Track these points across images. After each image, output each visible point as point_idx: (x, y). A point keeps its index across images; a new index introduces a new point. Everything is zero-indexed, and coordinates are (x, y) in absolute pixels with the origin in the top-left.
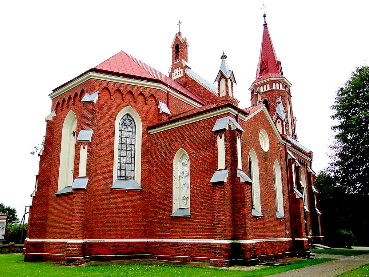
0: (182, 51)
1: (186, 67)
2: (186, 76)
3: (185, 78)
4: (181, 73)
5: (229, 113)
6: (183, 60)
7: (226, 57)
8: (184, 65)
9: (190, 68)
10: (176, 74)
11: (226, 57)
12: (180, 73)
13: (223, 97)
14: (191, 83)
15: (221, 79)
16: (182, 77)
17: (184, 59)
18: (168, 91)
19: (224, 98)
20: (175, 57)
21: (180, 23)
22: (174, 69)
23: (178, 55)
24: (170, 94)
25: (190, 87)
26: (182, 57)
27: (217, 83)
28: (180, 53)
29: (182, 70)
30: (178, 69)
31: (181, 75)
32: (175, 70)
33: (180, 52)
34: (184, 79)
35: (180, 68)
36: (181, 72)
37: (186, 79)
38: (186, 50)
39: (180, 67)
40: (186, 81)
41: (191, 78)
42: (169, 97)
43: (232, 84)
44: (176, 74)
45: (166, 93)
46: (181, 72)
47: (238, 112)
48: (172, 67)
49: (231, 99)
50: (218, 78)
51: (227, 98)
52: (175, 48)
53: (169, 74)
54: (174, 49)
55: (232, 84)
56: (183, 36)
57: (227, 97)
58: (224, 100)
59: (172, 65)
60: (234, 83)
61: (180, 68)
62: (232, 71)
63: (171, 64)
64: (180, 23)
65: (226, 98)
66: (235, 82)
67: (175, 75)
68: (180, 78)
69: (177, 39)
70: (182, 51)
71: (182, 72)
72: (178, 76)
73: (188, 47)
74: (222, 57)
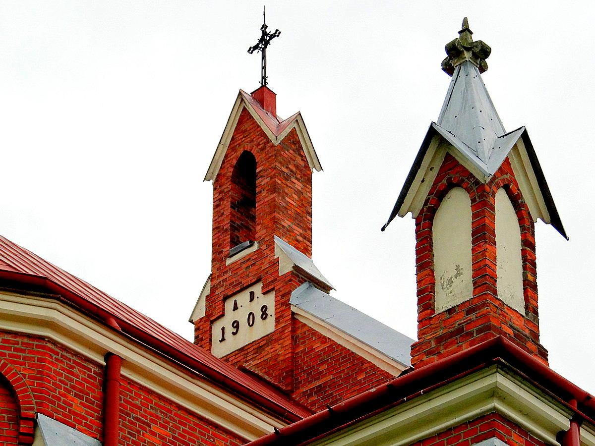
0: (274, 189)
1: (300, 276)
2: (294, 331)
3: (288, 342)
4: (264, 316)
5: (496, 414)
6: (277, 240)
7: (482, 53)
8: (285, 268)
9: (326, 288)
10: (236, 325)
11: (482, 53)
12: (258, 314)
13: (450, 311)
14: (326, 366)
15: (438, 196)
16: (268, 340)
17: (287, 234)
18: (109, 356)
19: (460, 320)
20: (233, 228)
21: (266, 38)
22: (226, 298)
23: (253, 219)
24: (124, 372)
25: (320, 389)
26: (275, 221)
27: (407, 224)
28: (264, 198)
29: (270, 301)
30: (246, 295)
31: (267, 327)
32: (229, 304)
33: (264, 194)
34: (282, 350)
35: (258, 289)
36: (264, 309)
37: (294, 346)
38: (299, 186)
39: (260, 285)
40: (294, 357)
41: (324, 340)
42: (121, 398)
43: (523, 228)
44: (236, 325)
45: (94, 369)
46: (264, 309)
47: (577, 420)
48: (213, 289)
49: (519, 324)
50: (421, 192)
51: (485, 315)
52: (235, 179)
53: (193, 327)
54: (227, 186)
55: (528, 245)
56: (284, 110)
57: (484, 305)
58: (460, 331)
59: (211, 278)
60: (543, 231)
61: (258, 289)
62: (525, 137)
63: (206, 269)
64: (266, 38)
65: (473, 316)
66: (556, 222)
67: (229, 330)
68: (258, 347)
69: (247, 126)
70: (274, 189)
71: (271, 311)
72: (247, 336)
73: (316, 176)
74: (453, 50)
